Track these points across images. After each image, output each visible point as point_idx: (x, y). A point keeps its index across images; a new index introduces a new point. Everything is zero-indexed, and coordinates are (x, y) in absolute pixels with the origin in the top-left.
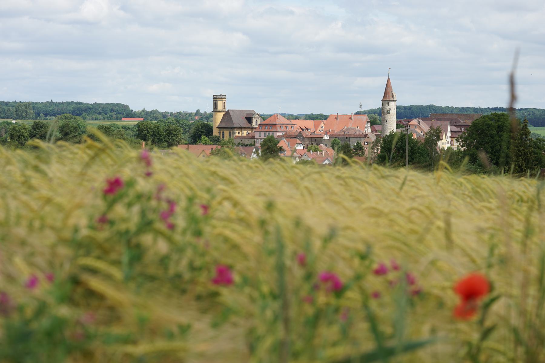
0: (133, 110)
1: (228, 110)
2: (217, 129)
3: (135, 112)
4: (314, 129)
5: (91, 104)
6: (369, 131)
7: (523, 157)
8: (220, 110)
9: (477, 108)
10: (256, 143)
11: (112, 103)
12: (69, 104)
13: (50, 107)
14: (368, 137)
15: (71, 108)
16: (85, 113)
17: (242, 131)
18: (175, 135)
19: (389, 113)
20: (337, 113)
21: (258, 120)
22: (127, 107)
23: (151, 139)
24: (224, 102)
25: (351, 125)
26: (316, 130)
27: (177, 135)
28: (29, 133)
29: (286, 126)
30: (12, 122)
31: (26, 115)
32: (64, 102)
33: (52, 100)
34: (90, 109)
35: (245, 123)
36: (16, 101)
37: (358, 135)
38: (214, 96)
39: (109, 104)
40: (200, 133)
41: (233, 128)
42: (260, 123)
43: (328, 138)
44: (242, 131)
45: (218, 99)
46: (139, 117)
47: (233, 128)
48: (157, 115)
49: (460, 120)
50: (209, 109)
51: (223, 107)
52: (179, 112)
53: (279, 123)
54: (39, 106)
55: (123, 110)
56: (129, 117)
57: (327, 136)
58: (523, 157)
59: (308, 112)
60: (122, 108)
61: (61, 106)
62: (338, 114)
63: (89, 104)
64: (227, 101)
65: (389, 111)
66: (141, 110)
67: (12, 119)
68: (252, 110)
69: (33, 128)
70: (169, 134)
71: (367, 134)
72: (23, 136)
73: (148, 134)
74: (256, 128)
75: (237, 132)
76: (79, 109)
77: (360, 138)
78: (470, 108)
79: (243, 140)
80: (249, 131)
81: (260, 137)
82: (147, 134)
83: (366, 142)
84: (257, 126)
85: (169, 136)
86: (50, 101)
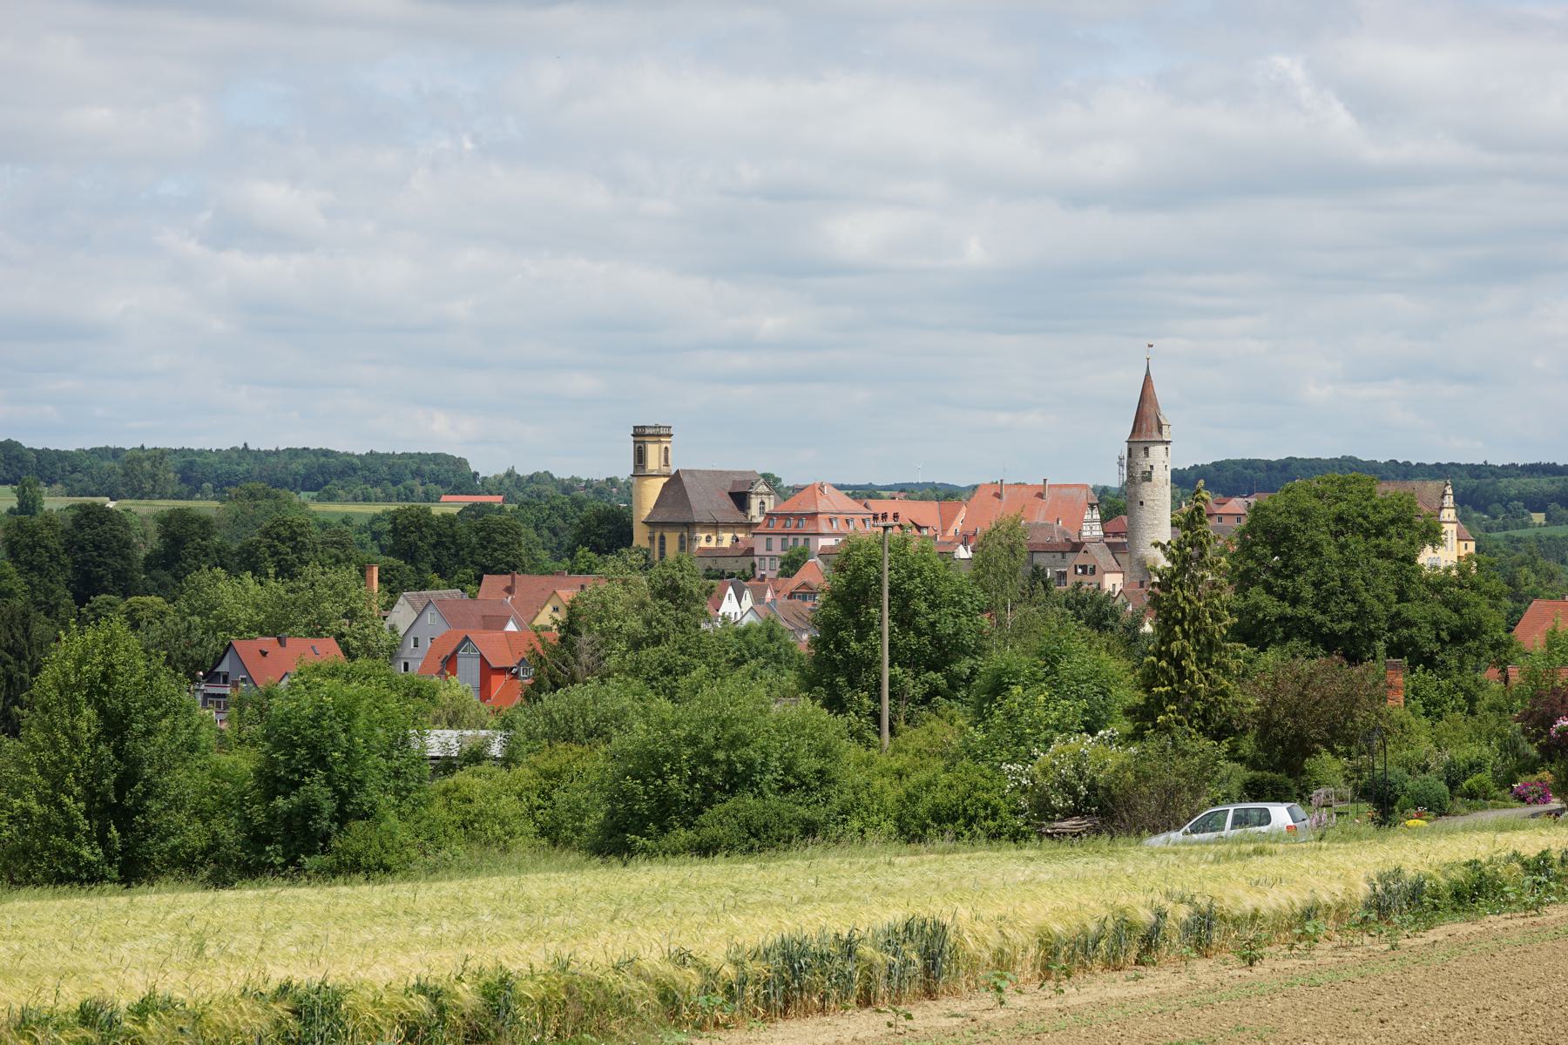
0: (477, 474)
1: (678, 471)
2: (645, 526)
3: (485, 478)
4: (938, 527)
5: (360, 457)
6: (1098, 533)
7: (1186, 627)
8: (653, 471)
9: (1479, 467)
10: (757, 569)
11: (419, 454)
12: (296, 455)
13: (238, 464)
14: (1085, 552)
15: (301, 467)
16: (336, 482)
17: (717, 533)
18: (502, 545)
19: (1149, 479)
20: (1045, 480)
21: (766, 501)
22: (460, 463)
23: (432, 557)
24: (664, 446)
25: (1041, 517)
26: (944, 531)
27: (511, 546)
28: (63, 541)
29: (849, 517)
30: (427, 511)
31: (154, 486)
32: (281, 448)
33: (245, 445)
34: (355, 470)
35: (728, 510)
36: (143, 447)
37: (1057, 545)
38: (635, 427)
39: (411, 456)
40: (593, 538)
41: (690, 526)
42: (772, 508)
43: (970, 555)
44: (717, 533)
45: (647, 439)
46: (491, 494)
47: (690, 526)
48: (542, 488)
49: (77, 500)
50: (623, 469)
51: (663, 463)
52: (611, 479)
53: (827, 509)
54: (206, 461)
55: (451, 474)
56: (462, 494)
57: (966, 550)
58: (1186, 627)
59: (840, 482)
60: (446, 467)
61: (273, 460)
62: (1048, 483)
63: (353, 455)
64: (673, 445)
65: (1150, 473)
66: (502, 471)
67: (108, 499)
68: (749, 470)
69: (77, 524)
70: (485, 543)
71: (1083, 543)
72: (46, 547)
73: (422, 541)
74: (757, 524)
75: (704, 536)
76: (323, 470)
77: (1063, 553)
78: (1458, 465)
79: (719, 560)
80: (740, 532)
81: (771, 550)
82: (420, 543)
83: (1080, 567)
84: (760, 519)
85: (485, 548)
86: (241, 446)
